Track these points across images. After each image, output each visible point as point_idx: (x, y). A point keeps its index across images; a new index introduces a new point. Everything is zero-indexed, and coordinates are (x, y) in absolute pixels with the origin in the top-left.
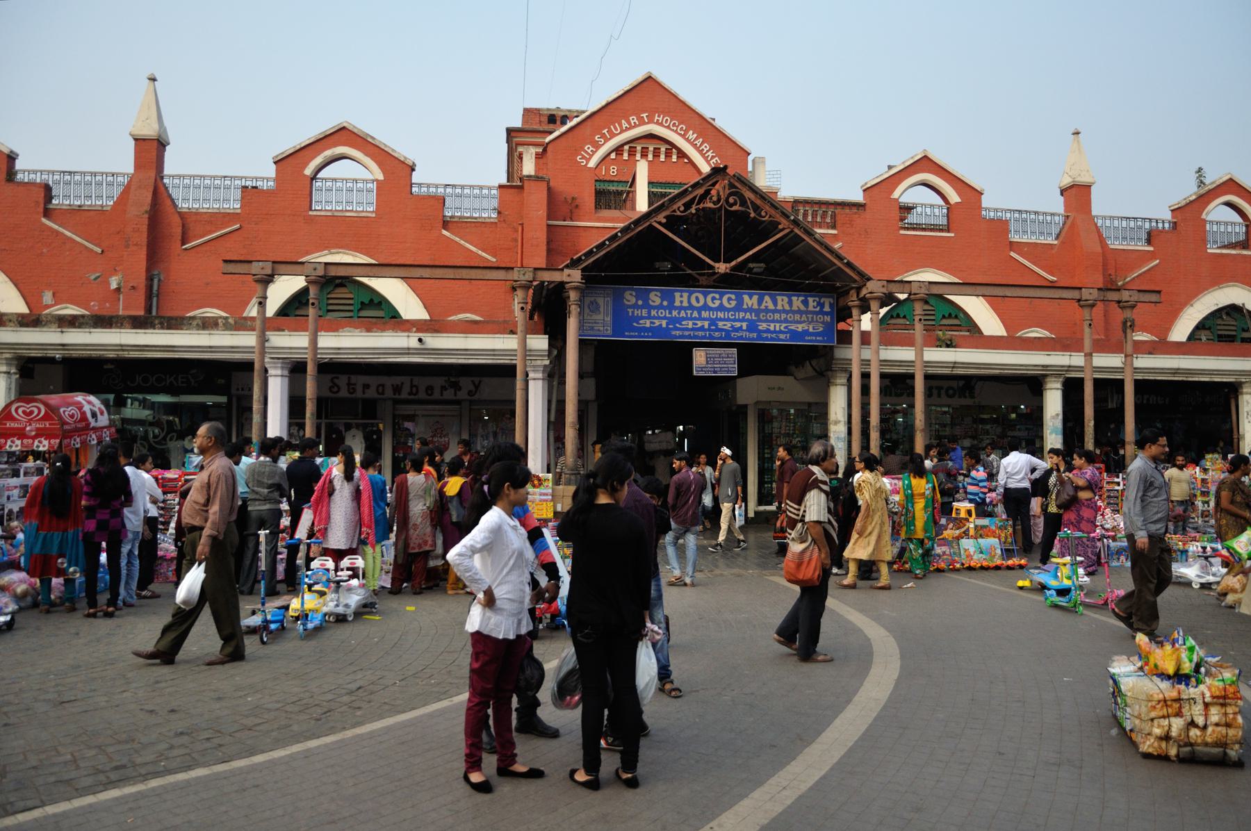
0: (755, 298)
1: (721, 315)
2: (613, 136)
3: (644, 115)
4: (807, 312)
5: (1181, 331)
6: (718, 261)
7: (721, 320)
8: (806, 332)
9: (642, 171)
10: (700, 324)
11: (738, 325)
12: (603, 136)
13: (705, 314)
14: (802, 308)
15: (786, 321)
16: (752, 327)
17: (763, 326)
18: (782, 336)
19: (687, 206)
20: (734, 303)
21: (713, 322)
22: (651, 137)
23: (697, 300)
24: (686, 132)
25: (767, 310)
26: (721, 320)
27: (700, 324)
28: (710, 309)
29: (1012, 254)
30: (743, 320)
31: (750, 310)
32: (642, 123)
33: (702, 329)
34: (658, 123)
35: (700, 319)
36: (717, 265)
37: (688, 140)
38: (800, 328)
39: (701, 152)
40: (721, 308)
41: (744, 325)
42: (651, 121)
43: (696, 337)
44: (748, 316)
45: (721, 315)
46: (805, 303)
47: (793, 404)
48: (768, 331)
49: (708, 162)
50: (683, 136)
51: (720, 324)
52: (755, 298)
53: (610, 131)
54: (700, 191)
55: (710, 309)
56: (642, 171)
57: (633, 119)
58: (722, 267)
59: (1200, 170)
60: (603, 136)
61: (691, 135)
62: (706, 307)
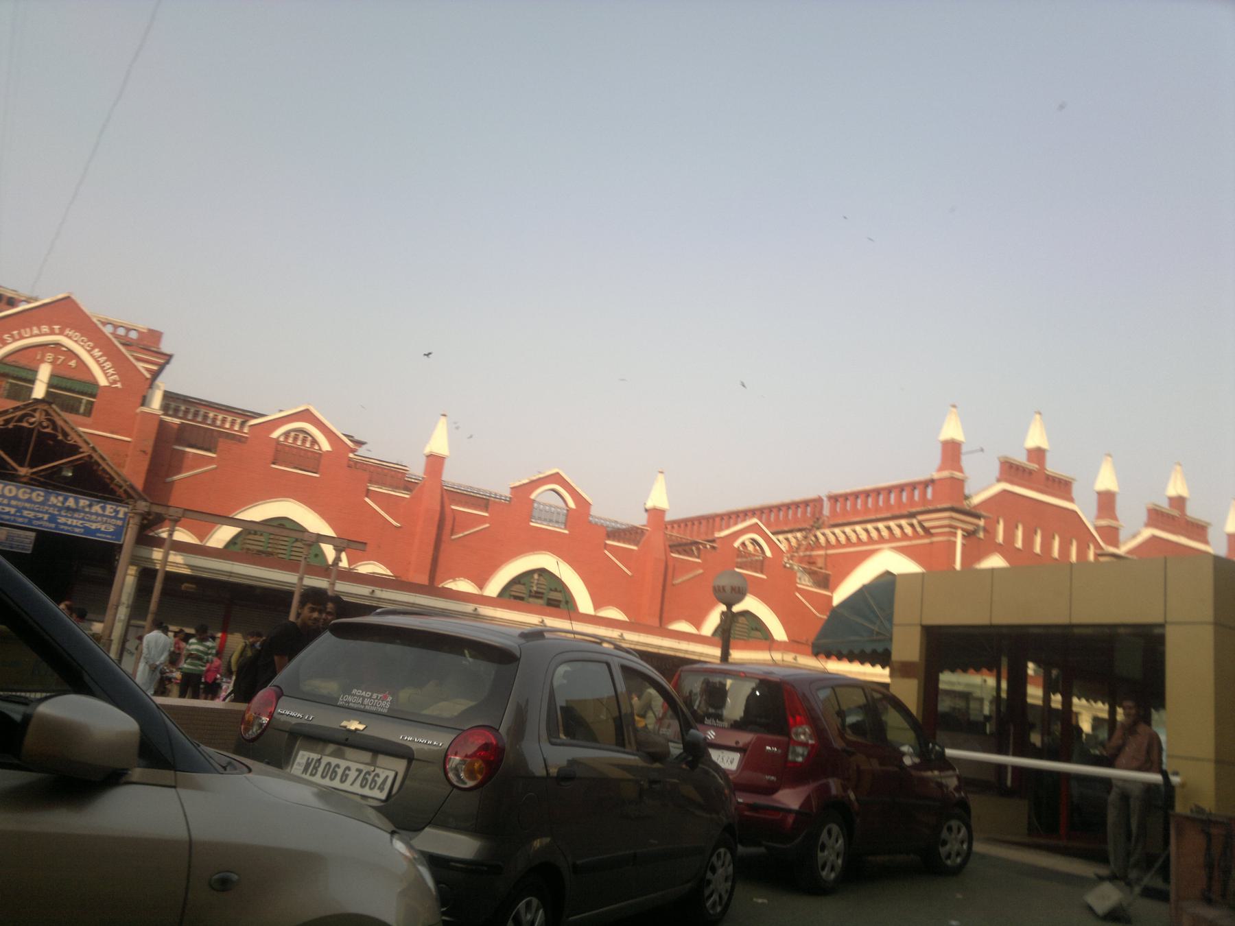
0: (61, 498)
1: (27, 505)
2: (22, 338)
3: (56, 327)
4: (104, 516)
5: (494, 587)
6: (21, 465)
7: (26, 509)
8: (98, 530)
9: (44, 373)
10: (7, 509)
11: (40, 515)
12: (12, 336)
13: (14, 503)
14: (100, 511)
15: (83, 519)
16: (53, 519)
17: (62, 520)
18: (77, 530)
19: (7, 422)
20: (41, 499)
21: (19, 509)
22: (58, 344)
23: (10, 491)
24: (93, 348)
25: (68, 509)
26: (26, 509)
27: (7, 509)
28: (19, 500)
29: (367, 500)
30: (46, 513)
31: (54, 506)
32: (52, 333)
33: (8, 513)
34: (67, 336)
35: (9, 505)
36: (20, 469)
37: (92, 356)
38: (94, 526)
39: (102, 368)
40: (29, 500)
41: (46, 517)
42: (61, 333)
43: (15, 521)
44: (51, 510)
45: (27, 505)
46: (103, 509)
47: (754, 690)
48: (65, 524)
49: (107, 377)
50: (89, 351)
51: (25, 513)
52: (61, 498)
53: (20, 334)
54: (19, 413)
55: (19, 500)
56: (44, 373)
57: (35, 331)
58: (23, 471)
59: (982, 450)
60: (12, 336)
61: (97, 352)
62: (16, 498)
